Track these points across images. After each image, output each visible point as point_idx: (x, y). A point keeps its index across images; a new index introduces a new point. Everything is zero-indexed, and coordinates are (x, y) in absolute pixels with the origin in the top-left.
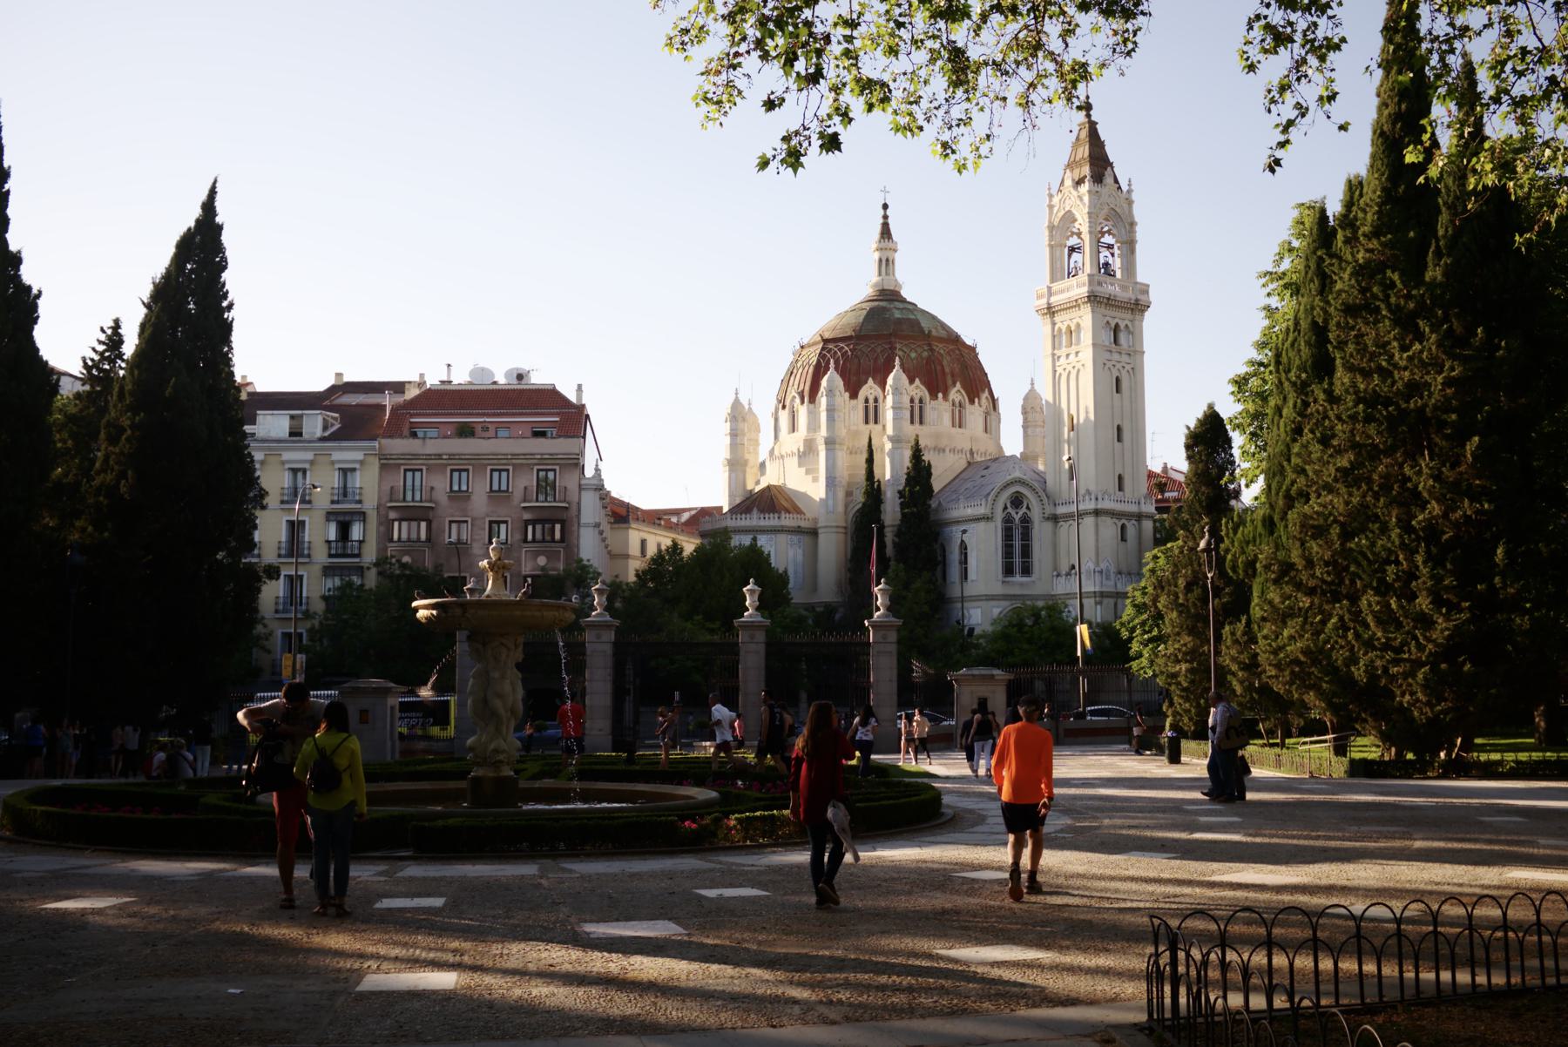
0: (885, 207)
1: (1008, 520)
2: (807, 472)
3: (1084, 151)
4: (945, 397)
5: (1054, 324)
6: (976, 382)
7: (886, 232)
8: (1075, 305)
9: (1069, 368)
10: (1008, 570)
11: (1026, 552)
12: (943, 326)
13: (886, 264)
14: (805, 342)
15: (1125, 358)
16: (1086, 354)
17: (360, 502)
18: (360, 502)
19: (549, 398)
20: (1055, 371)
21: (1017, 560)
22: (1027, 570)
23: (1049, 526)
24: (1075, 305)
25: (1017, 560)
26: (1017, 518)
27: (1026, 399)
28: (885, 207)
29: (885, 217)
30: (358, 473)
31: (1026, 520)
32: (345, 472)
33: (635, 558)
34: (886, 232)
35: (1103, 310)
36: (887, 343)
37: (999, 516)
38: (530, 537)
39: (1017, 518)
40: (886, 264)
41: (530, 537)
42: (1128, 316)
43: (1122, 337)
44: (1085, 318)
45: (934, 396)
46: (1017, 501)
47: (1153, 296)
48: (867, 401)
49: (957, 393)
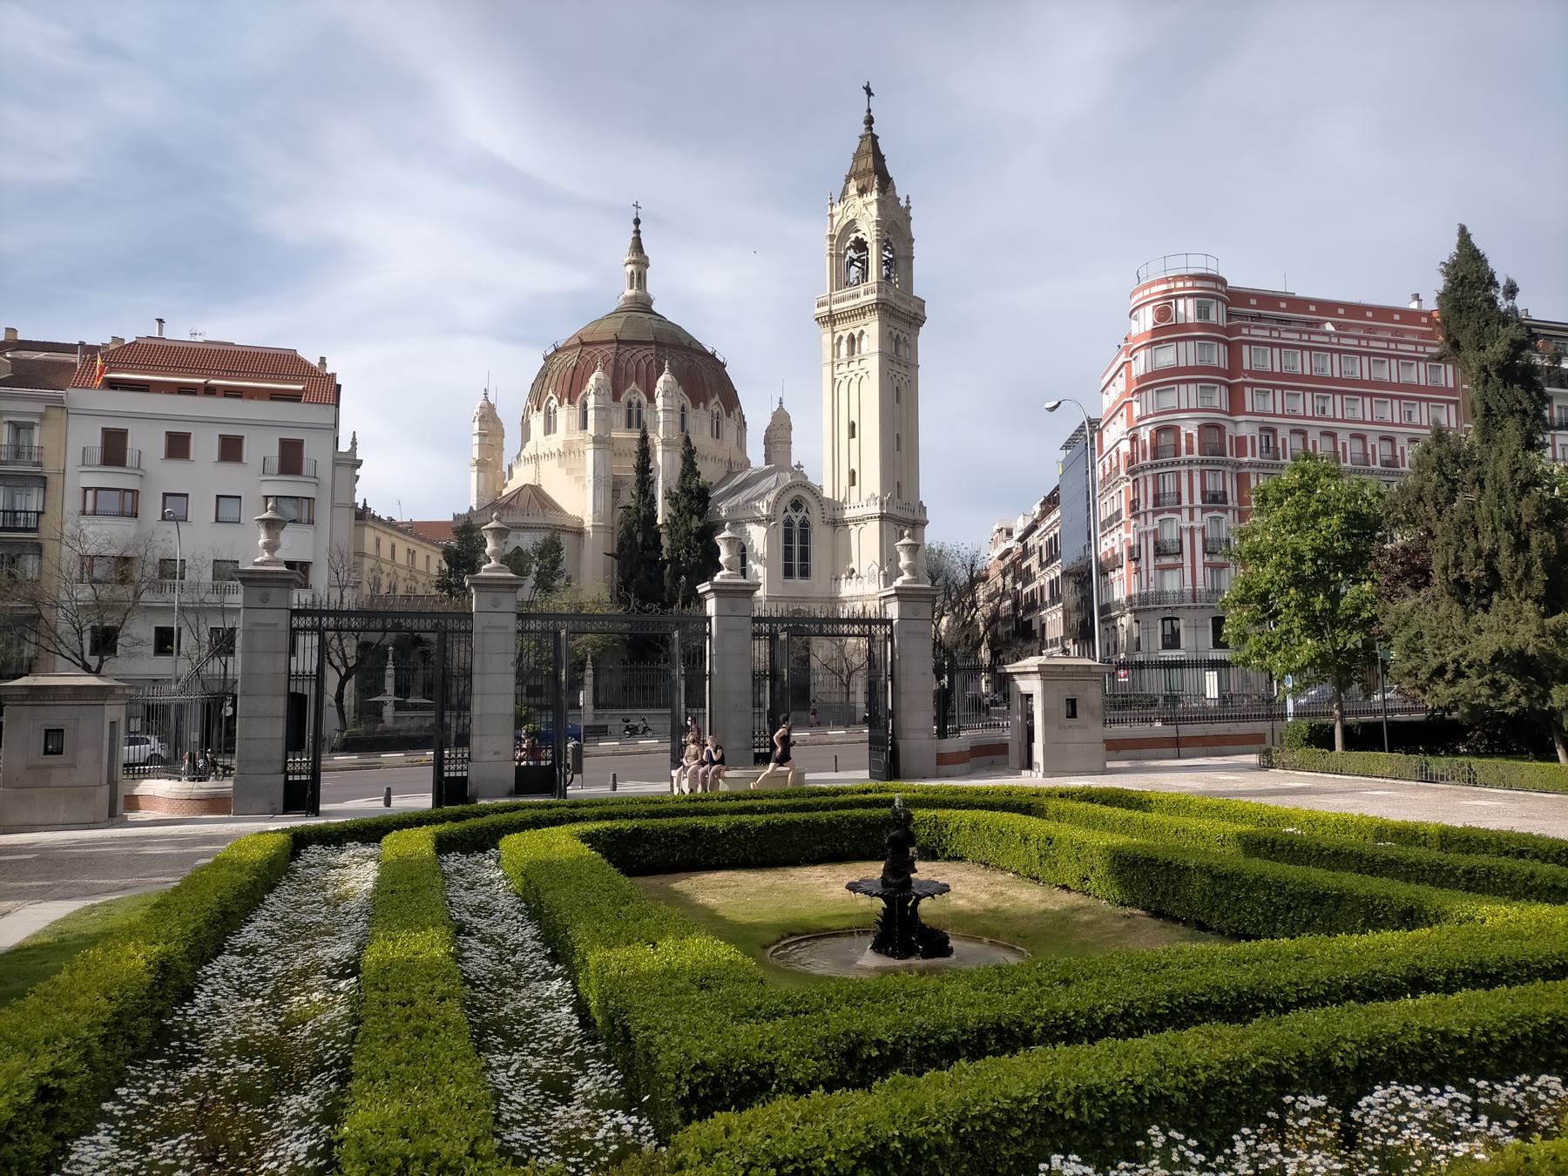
0: (637, 222)
1: (788, 523)
2: (569, 472)
3: (867, 146)
4: (705, 407)
5: (834, 333)
6: (731, 400)
7: (638, 246)
8: (861, 312)
9: (851, 375)
10: (788, 573)
11: (805, 555)
12: (692, 340)
13: (639, 279)
14: (560, 345)
15: (903, 370)
16: (872, 364)
17: (39, 464)
18: (39, 464)
19: (284, 363)
20: (834, 380)
21: (796, 563)
22: (805, 573)
23: (829, 529)
24: (861, 312)
25: (796, 563)
26: (797, 521)
27: (775, 416)
28: (637, 222)
29: (638, 232)
30: (37, 429)
31: (805, 524)
32: (17, 428)
33: (370, 557)
34: (638, 246)
35: (894, 323)
36: (645, 358)
37: (782, 518)
38: (89, 507)
39: (797, 521)
40: (639, 279)
41: (89, 507)
42: (906, 329)
43: (901, 347)
44: (871, 328)
45: (695, 406)
46: (797, 505)
47: (929, 311)
48: (630, 404)
49: (715, 404)
